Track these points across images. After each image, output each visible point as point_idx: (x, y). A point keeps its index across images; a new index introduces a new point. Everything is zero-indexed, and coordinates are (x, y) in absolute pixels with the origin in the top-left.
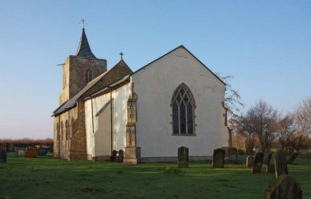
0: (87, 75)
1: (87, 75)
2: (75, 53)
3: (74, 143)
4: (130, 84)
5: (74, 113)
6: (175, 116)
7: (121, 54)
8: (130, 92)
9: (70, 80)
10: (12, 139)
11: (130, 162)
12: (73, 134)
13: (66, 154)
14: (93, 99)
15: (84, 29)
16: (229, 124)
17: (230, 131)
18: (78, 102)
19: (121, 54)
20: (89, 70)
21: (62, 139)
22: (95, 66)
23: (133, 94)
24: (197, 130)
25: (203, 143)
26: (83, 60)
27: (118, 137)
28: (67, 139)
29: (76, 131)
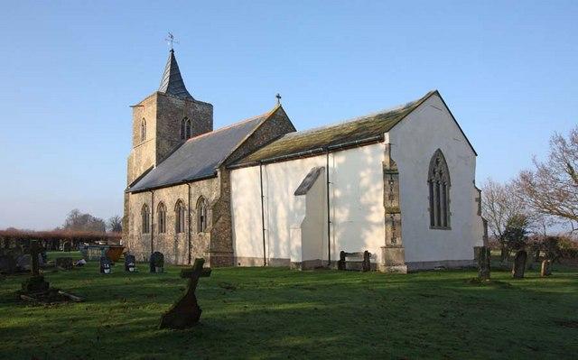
0: (183, 127)
1: (183, 127)
2: (164, 90)
3: (215, 239)
4: (382, 146)
5: (210, 190)
6: (431, 198)
7: (279, 97)
8: (383, 158)
9: (158, 133)
10: (36, 231)
11: (397, 271)
12: (215, 222)
13: (382, 269)
14: (263, 167)
15: (173, 51)
16: (486, 211)
17: (485, 223)
18: (221, 171)
19: (279, 97)
20: (186, 118)
21: (162, 229)
22: (196, 113)
23: (391, 162)
24: (453, 221)
25: (458, 244)
26: (178, 102)
27: (338, 234)
28: (178, 230)
29: (218, 219)
